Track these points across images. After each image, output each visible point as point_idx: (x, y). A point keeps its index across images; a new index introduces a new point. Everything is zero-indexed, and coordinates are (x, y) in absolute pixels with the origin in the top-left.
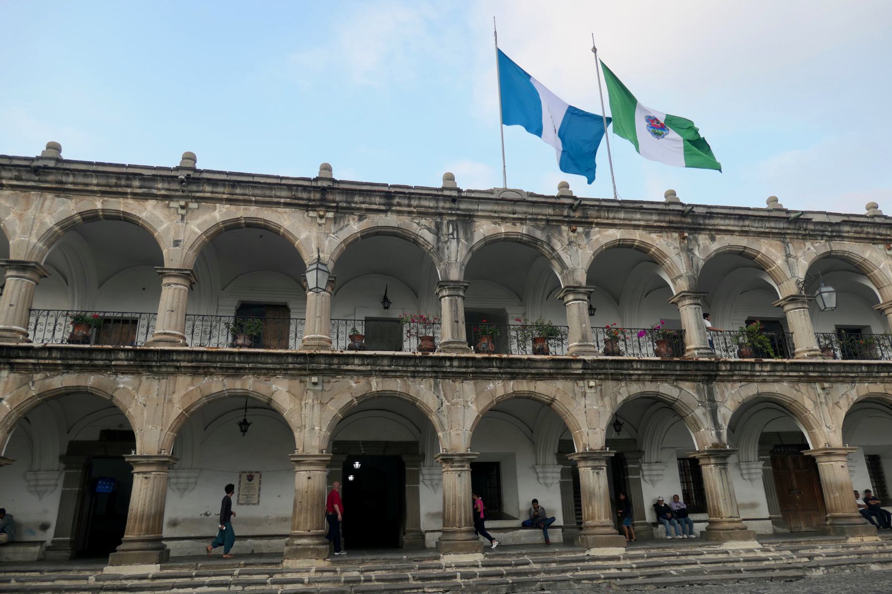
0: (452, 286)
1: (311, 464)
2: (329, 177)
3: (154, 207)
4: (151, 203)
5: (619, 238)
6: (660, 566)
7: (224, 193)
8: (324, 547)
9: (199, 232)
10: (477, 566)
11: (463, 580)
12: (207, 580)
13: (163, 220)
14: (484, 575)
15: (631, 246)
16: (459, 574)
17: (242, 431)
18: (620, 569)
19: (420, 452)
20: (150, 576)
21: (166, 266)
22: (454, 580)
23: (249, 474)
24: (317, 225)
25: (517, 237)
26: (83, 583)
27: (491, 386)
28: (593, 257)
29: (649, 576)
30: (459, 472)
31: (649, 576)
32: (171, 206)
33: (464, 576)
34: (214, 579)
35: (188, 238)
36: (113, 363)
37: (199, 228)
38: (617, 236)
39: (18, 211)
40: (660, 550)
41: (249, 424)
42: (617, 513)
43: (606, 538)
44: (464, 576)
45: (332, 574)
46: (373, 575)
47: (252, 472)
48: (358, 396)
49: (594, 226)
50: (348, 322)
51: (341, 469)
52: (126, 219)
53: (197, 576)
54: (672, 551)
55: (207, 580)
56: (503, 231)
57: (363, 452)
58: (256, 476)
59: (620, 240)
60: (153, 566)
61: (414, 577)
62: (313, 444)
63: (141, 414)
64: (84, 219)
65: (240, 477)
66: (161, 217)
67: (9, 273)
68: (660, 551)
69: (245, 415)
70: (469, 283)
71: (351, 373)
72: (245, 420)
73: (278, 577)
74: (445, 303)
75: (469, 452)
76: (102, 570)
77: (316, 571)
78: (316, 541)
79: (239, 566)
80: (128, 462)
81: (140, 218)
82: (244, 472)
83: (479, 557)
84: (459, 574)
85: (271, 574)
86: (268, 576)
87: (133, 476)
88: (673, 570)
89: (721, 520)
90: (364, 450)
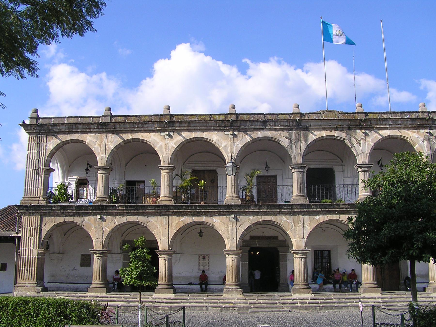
0: (298, 167)
1: (233, 254)
2: (234, 112)
3: (154, 135)
4: (152, 134)
5: (389, 135)
6: (394, 302)
7: (184, 126)
8: (241, 290)
9: (176, 147)
10: (308, 299)
11: (301, 305)
12: (194, 301)
13: (159, 142)
14: (309, 303)
15: (397, 138)
16: (299, 302)
17: (200, 236)
18: (374, 303)
19: (287, 246)
20: (172, 298)
21: (162, 165)
22: (297, 305)
23: (203, 256)
24: (229, 139)
25: (332, 137)
26: (148, 300)
27: (317, 217)
28: (374, 147)
29: (386, 306)
30: (301, 258)
31: (386, 306)
32: (161, 134)
33: (301, 303)
34: (196, 300)
35: (171, 150)
36: (146, 211)
37: (175, 145)
38: (388, 134)
39: (99, 143)
40: (398, 295)
41: (203, 233)
42: (207, 281)
43: (371, 289)
44: (301, 303)
45: (244, 300)
46: (261, 302)
47: (204, 255)
48: (253, 223)
49: (375, 128)
50: (286, 186)
51: (247, 254)
52: (142, 141)
53: (189, 299)
54: (403, 296)
55: (194, 301)
56: (325, 135)
57: (258, 245)
58: (207, 257)
59: (389, 136)
60: (172, 295)
61: (279, 303)
62: (234, 245)
63: (159, 233)
64: (125, 144)
65: (199, 257)
66: (158, 140)
67: (99, 172)
68: (392, 296)
69: (201, 228)
70: (306, 165)
71: (249, 213)
72: (201, 231)
73: (222, 301)
74: (295, 175)
75: (306, 249)
76: (153, 295)
77: (238, 299)
78: (237, 287)
79: (206, 296)
80: (157, 253)
81: (148, 141)
82: (201, 255)
83: (309, 296)
84: (299, 302)
85: (219, 300)
86: (218, 300)
87: (159, 259)
88: (399, 304)
89: (435, 282)
90: (258, 245)
